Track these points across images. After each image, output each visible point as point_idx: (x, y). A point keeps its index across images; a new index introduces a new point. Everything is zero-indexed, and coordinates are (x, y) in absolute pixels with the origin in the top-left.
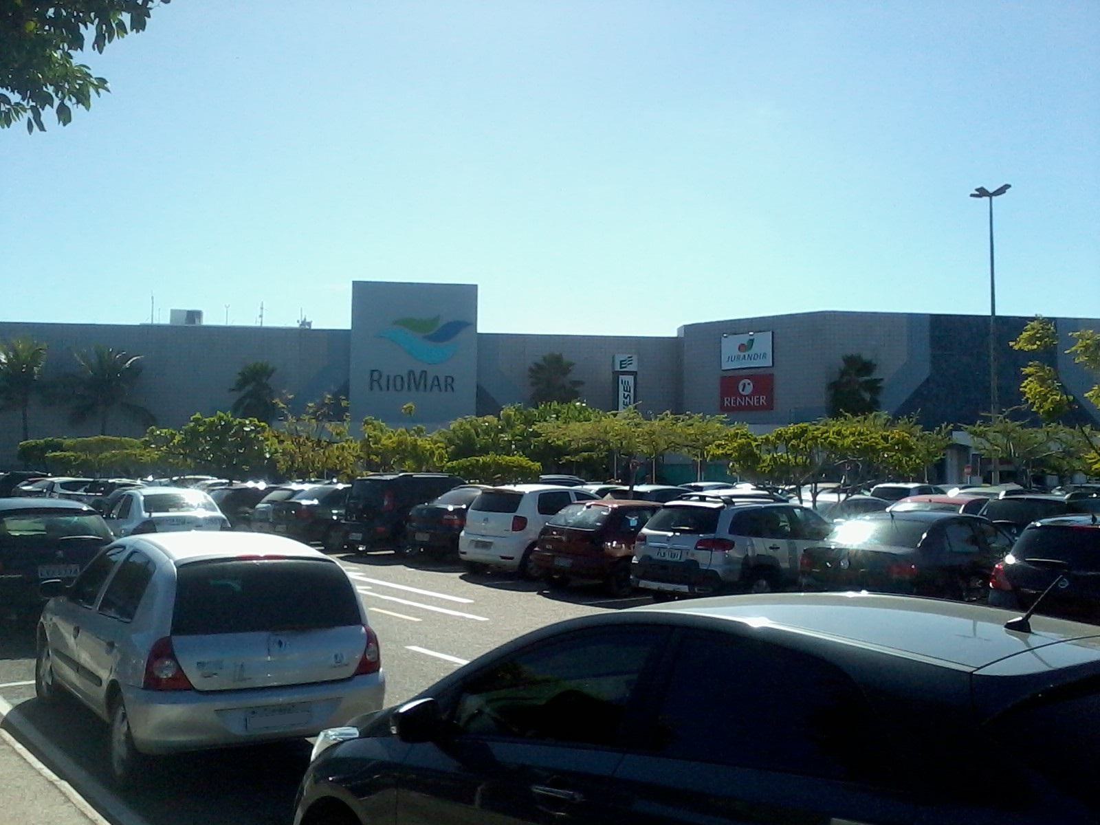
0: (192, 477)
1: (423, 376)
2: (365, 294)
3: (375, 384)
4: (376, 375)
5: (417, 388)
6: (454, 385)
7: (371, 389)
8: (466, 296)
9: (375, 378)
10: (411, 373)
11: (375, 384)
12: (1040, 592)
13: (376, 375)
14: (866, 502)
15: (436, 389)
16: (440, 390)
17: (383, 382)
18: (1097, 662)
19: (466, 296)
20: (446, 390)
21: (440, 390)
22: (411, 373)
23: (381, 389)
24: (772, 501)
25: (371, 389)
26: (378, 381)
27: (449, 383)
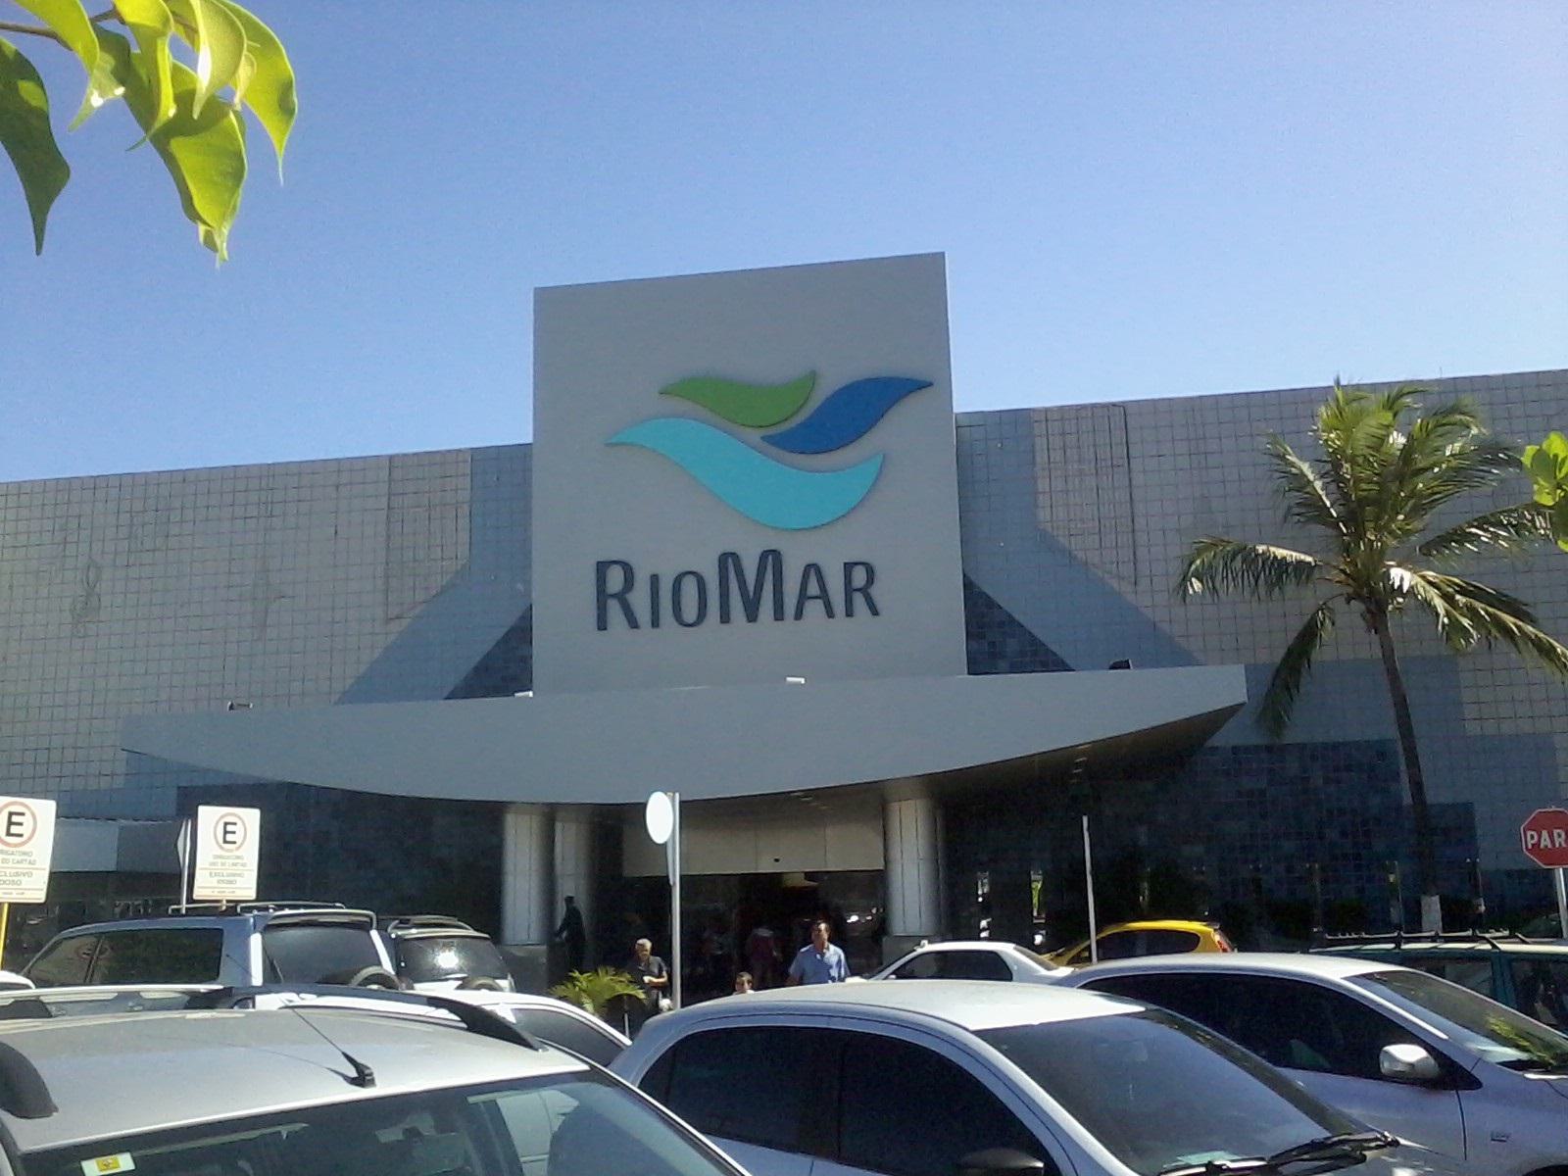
0: (1541, 1024)
1: (813, 588)
2: (568, 319)
3: (614, 608)
4: (615, 579)
5: (752, 616)
6: (874, 591)
7: (602, 625)
8: (916, 285)
9: (613, 591)
10: (728, 561)
11: (614, 608)
12: (1291, 452)
13: (615, 579)
14: (1468, 937)
15: (815, 608)
16: (830, 613)
17: (640, 599)
18: (1566, 370)
19: (916, 285)
20: (849, 613)
21: (830, 614)
22: (728, 561)
23: (633, 623)
24: (458, 1019)
25: (602, 625)
26: (621, 597)
27: (860, 586)
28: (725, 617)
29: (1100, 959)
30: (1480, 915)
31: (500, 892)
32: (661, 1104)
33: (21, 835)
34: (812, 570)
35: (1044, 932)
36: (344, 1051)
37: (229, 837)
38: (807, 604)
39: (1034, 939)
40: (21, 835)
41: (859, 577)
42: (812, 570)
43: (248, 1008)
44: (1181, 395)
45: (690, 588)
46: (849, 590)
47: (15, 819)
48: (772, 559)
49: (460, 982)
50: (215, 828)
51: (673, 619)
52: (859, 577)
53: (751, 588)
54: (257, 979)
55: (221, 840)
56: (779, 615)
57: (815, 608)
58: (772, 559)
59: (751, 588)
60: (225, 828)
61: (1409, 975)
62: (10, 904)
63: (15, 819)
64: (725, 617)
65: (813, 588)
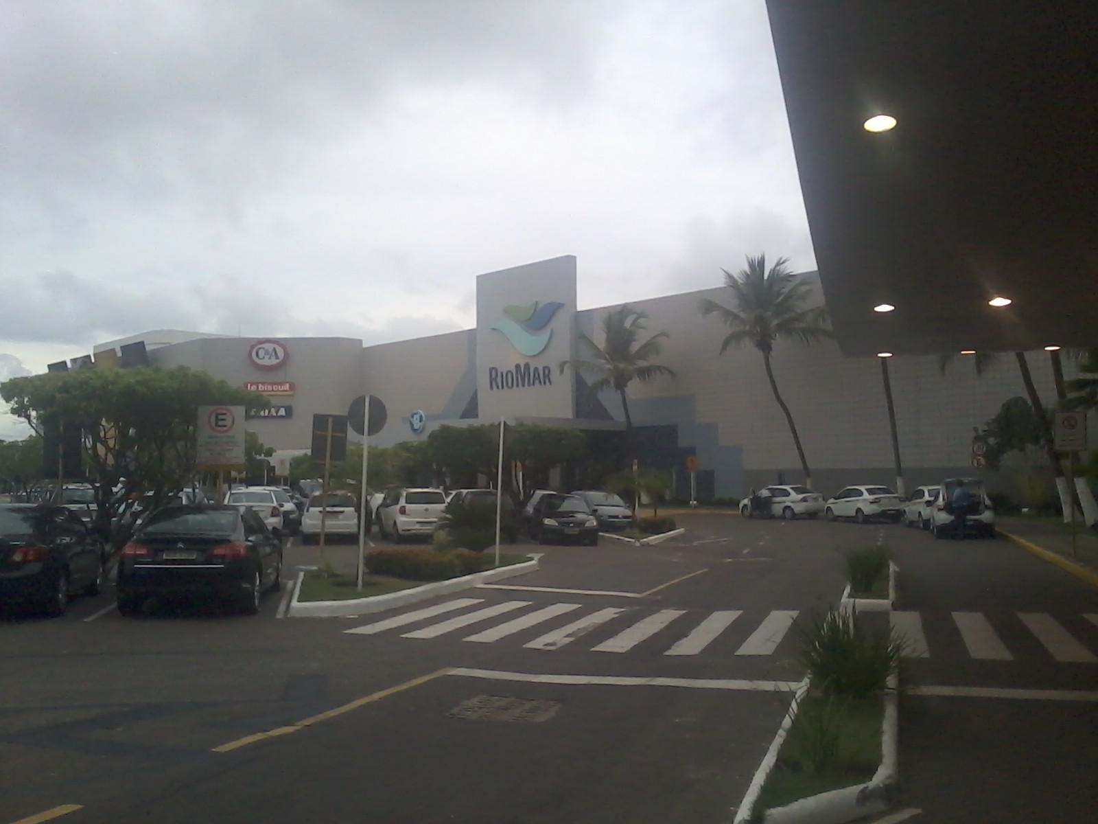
6: (551, 376)
7: (491, 387)
19: (564, 269)
22: (518, 366)
23: (498, 387)
28: (518, 385)
30: (686, 530)
32: (496, 527)
33: (225, 426)
34: (536, 369)
35: (343, 480)
37: (220, 423)
40: (225, 426)
41: (547, 372)
42: (536, 369)
47: (220, 417)
48: (527, 366)
50: (210, 417)
54: (233, 492)
55: (214, 424)
56: (529, 385)
57: (537, 382)
58: (527, 366)
60: (217, 417)
61: (617, 541)
63: (220, 417)
64: (518, 385)
65: (537, 375)
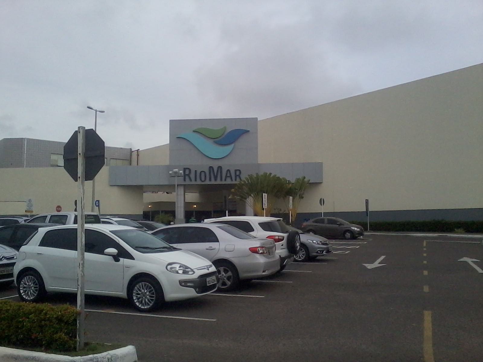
1: (228, 175)
10: (211, 168)
22: (211, 168)
29: (228, 216)
31: (64, 257)
36: (93, 110)
38: (227, 178)
39: (425, 253)
41: (238, 173)
43: (225, 216)
44: (478, 64)
45: (203, 174)
46: (236, 176)
49: (357, 238)
51: (206, 172)
52: (238, 173)
53: (216, 174)
58: (220, 168)
59: (216, 174)
62: (195, 211)
65: (228, 175)
